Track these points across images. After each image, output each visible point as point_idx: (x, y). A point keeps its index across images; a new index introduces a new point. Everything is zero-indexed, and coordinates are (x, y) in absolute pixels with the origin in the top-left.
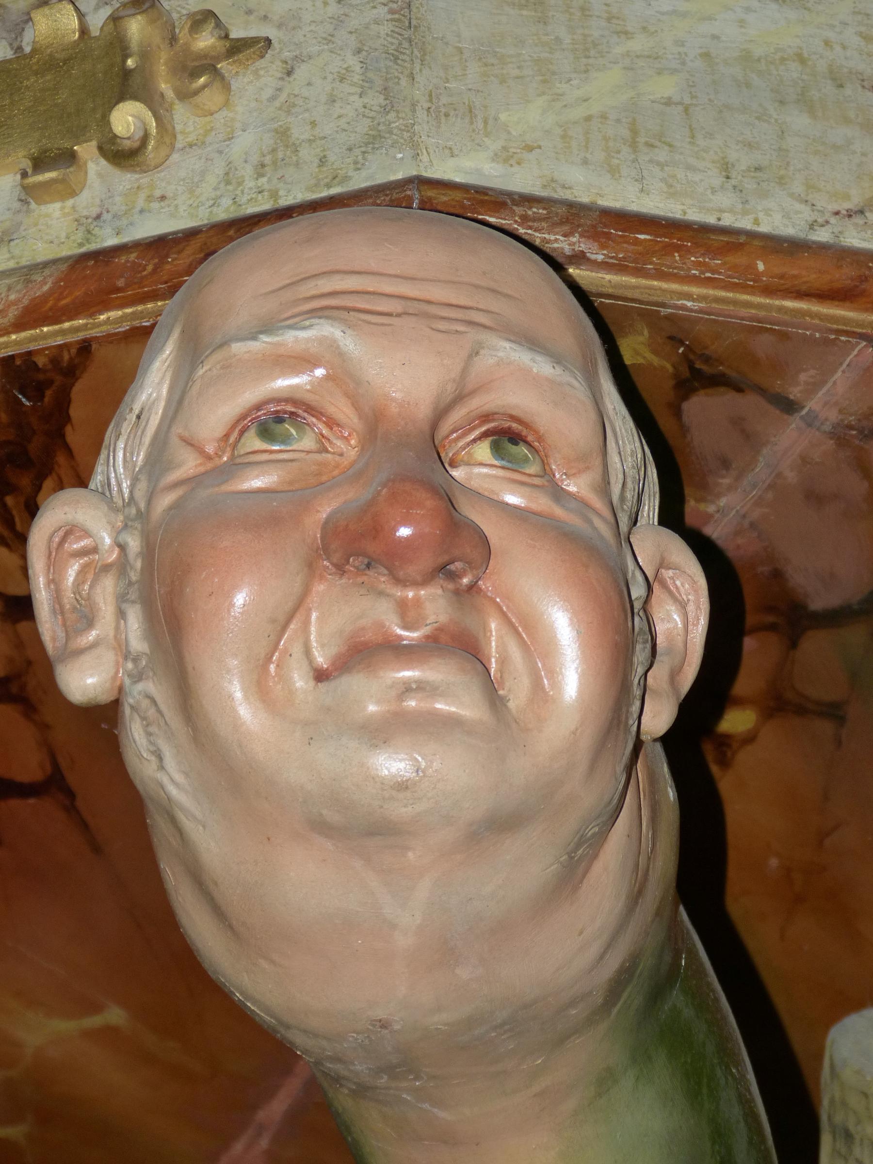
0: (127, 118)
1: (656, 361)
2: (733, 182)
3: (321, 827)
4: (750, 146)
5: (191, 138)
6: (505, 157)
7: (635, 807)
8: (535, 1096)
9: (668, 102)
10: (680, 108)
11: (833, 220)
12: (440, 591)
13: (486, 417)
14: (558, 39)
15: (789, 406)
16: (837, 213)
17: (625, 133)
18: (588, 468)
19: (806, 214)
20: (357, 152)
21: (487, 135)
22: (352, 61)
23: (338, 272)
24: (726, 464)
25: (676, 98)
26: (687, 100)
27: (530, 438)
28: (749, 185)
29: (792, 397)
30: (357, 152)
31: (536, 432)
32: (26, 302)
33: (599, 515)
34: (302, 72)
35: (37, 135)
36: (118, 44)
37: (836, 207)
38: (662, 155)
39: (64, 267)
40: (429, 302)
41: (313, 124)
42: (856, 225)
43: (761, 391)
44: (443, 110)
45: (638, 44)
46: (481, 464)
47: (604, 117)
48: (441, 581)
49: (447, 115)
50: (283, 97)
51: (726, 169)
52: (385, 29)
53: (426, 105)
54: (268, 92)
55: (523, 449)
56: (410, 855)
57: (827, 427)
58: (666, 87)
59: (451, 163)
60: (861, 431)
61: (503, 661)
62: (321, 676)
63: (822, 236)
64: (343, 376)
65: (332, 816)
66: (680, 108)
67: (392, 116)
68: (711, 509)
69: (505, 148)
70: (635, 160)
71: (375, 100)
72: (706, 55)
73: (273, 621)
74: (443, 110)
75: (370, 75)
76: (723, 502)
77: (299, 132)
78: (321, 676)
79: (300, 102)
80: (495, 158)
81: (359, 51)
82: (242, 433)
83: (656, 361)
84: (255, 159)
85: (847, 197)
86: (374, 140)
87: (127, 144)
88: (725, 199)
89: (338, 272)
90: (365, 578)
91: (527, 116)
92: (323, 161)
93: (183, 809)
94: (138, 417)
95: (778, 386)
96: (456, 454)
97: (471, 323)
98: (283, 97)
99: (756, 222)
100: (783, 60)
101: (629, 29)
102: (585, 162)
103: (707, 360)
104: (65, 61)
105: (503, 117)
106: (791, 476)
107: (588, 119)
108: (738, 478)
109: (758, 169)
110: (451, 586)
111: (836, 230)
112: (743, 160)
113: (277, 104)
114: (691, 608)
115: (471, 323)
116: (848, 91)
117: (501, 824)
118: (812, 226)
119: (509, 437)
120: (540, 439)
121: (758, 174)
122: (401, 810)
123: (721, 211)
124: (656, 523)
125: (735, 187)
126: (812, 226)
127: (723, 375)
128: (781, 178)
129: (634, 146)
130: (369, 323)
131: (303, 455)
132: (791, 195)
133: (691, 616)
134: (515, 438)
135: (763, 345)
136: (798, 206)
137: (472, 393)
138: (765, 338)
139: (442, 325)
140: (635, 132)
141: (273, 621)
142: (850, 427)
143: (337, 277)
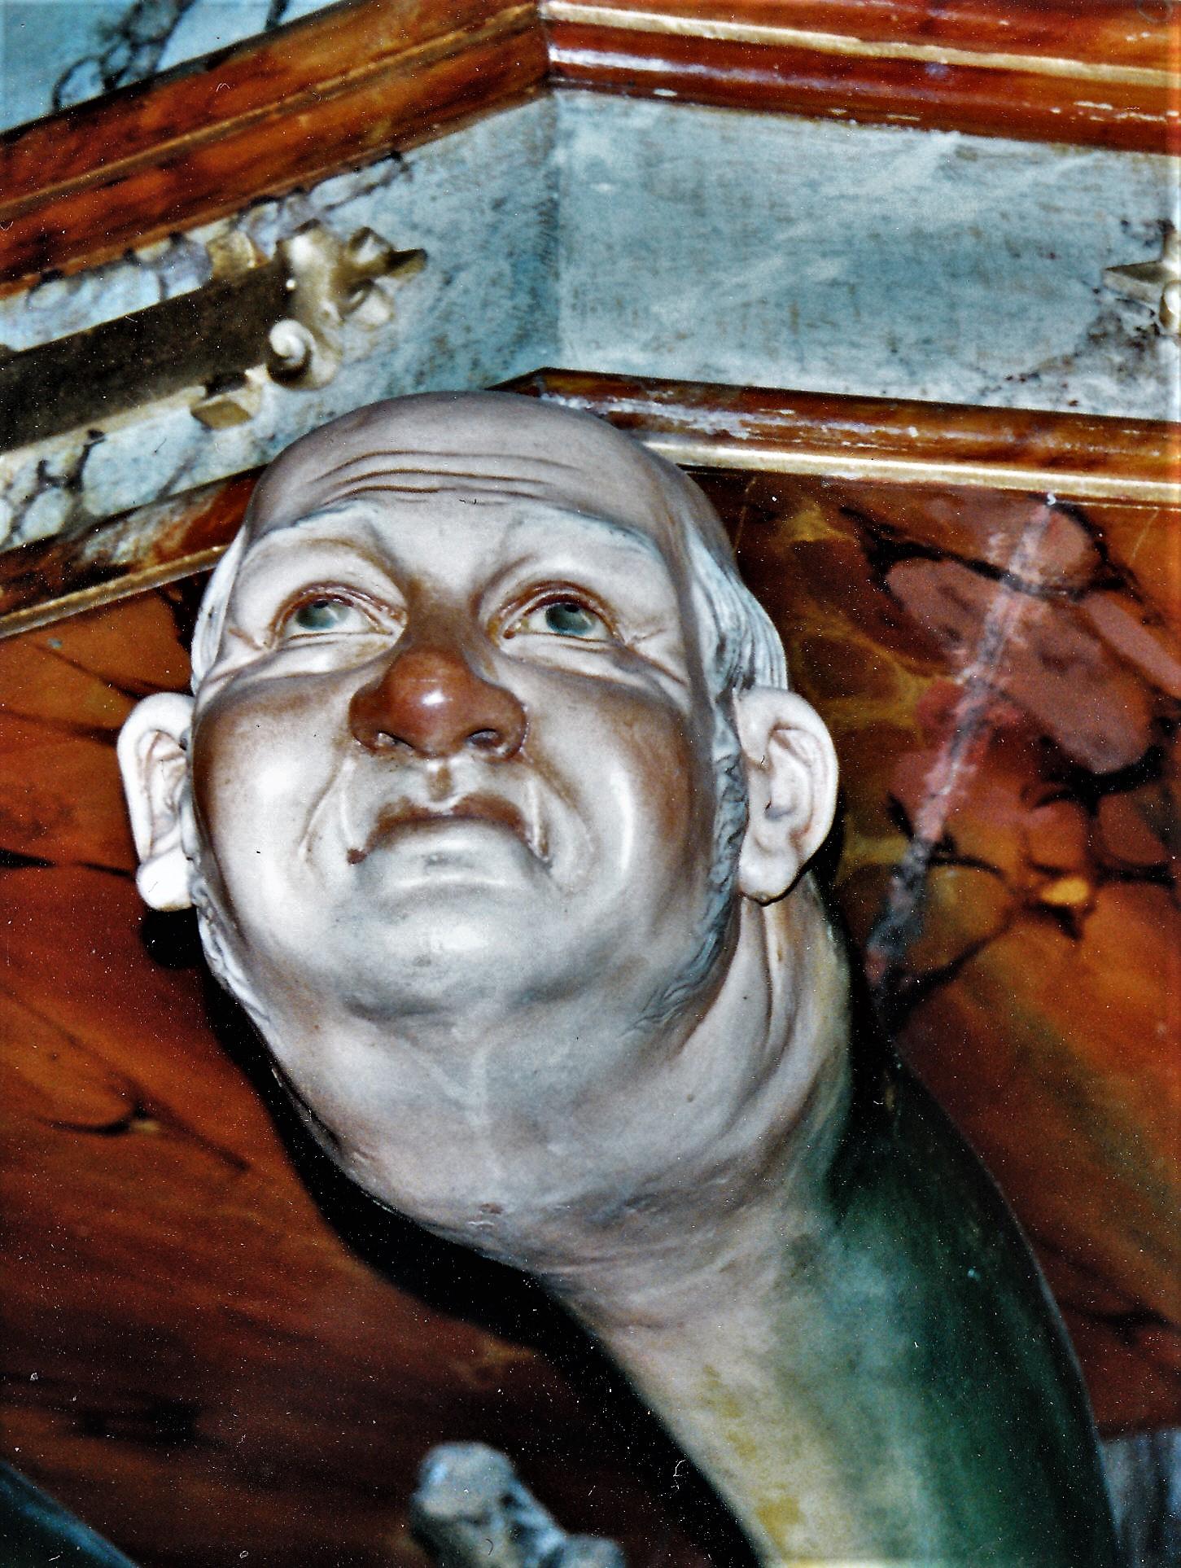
0: (286, 337)
1: (840, 536)
2: (899, 355)
3: (359, 1010)
4: (918, 319)
5: (358, 353)
6: (656, 346)
7: (757, 970)
8: (722, 1270)
9: (834, 283)
10: (845, 289)
11: (1006, 385)
12: (471, 761)
13: (545, 585)
14: (715, 230)
15: (994, 573)
16: (1010, 378)
17: (785, 314)
18: (660, 631)
19: (979, 382)
20: (506, 351)
21: (635, 326)
22: (505, 266)
23: (379, 454)
24: (955, 636)
25: (842, 278)
26: (853, 280)
27: (592, 603)
28: (917, 357)
29: (991, 562)
30: (506, 351)
31: (596, 597)
32: (189, 523)
33: (676, 679)
34: (464, 279)
35: (212, 363)
36: (283, 267)
37: (1008, 373)
38: (824, 334)
39: (222, 487)
40: (471, 476)
41: (468, 329)
42: (1030, 389)
43: (957, 558)
44: (589, 305)
45: (802, 229)
46: (536, 633)
47: (763, 302)
48: (472, 752)
49: (593, 310)
50: (443, 304)
51: (893, 346)
52: (533, 232)
53: (572, 301)
54: (429, 303)
55: (582, 616)
56: (454, 1030)
57: (1035, 589)
58: (830, 269)
59: (599, 354)
60: (1070, 590)
61: (546, 828)
62: (355, 857)
63: (994, 401)
64: (383, 558)
65: (368, 999)
66: (845, 289)
67: (538, 315)
68: (959, 681)
69: (656, 338)
70: (795, 342)
71: (523, 300)
72: (875, 236)
73: (296, 803)
74: (589, 305)
75: (521, 277)
76: (967, 672)
77: (456, 338)
78: (355, 857)
79: (457, 309)
80: (645, 347)
81: (511, 254)
82: (285, 620)
83: (840, 536)
84: (415, 367)
85: (1022, 362)
86: (523, 339)
87: (292, 363)
88: (891, 373)
89: (379, 454)
90: (394, 754)
91: (678, 307)
92: (476, 364)
93: (253, 1009)
94: (210, 615)
95: (971, 551)
96: (511, 626)
97: (515, 494)
98: (443, 304)
99: (924, 392)
100: (957, 235)
101: (793, 215)
102: (742, 346)
103: (892, 529)
104: (241, 290)
105: (655, 309)
106: (1021, 642)
107: (746, 305)
108: (973, 647)
109: (927, 341)
110: (483, 755)
111: (1009, 394)
112: (910, 333)
113: (436, 313)
114: (818, 768)
115: (515, 494)
116: (1025, 261)
117: (544, 993)
118: (983, 392)
119: (567, 606)
120: (603, 603)
121: (928, 347)
122: (429, 987)
123: (887, 384)
124: (785, 686)
125: (901, 360)
126: (983, 392)
127: (911, 544)
128: (953, 347)
129: (794, 327)
130: (403, 501)
131: (344, 637)
132: (963, 365)
133: (819, 776)
134: (575, 605)
135: (938, 510)
136: (967, 374)
137: (521, 562)
138: (939, 504)
139: (481, 498)
140: (795, 314)
141: (296, 803)
142: (1058, 588)
143: (378, 459)
